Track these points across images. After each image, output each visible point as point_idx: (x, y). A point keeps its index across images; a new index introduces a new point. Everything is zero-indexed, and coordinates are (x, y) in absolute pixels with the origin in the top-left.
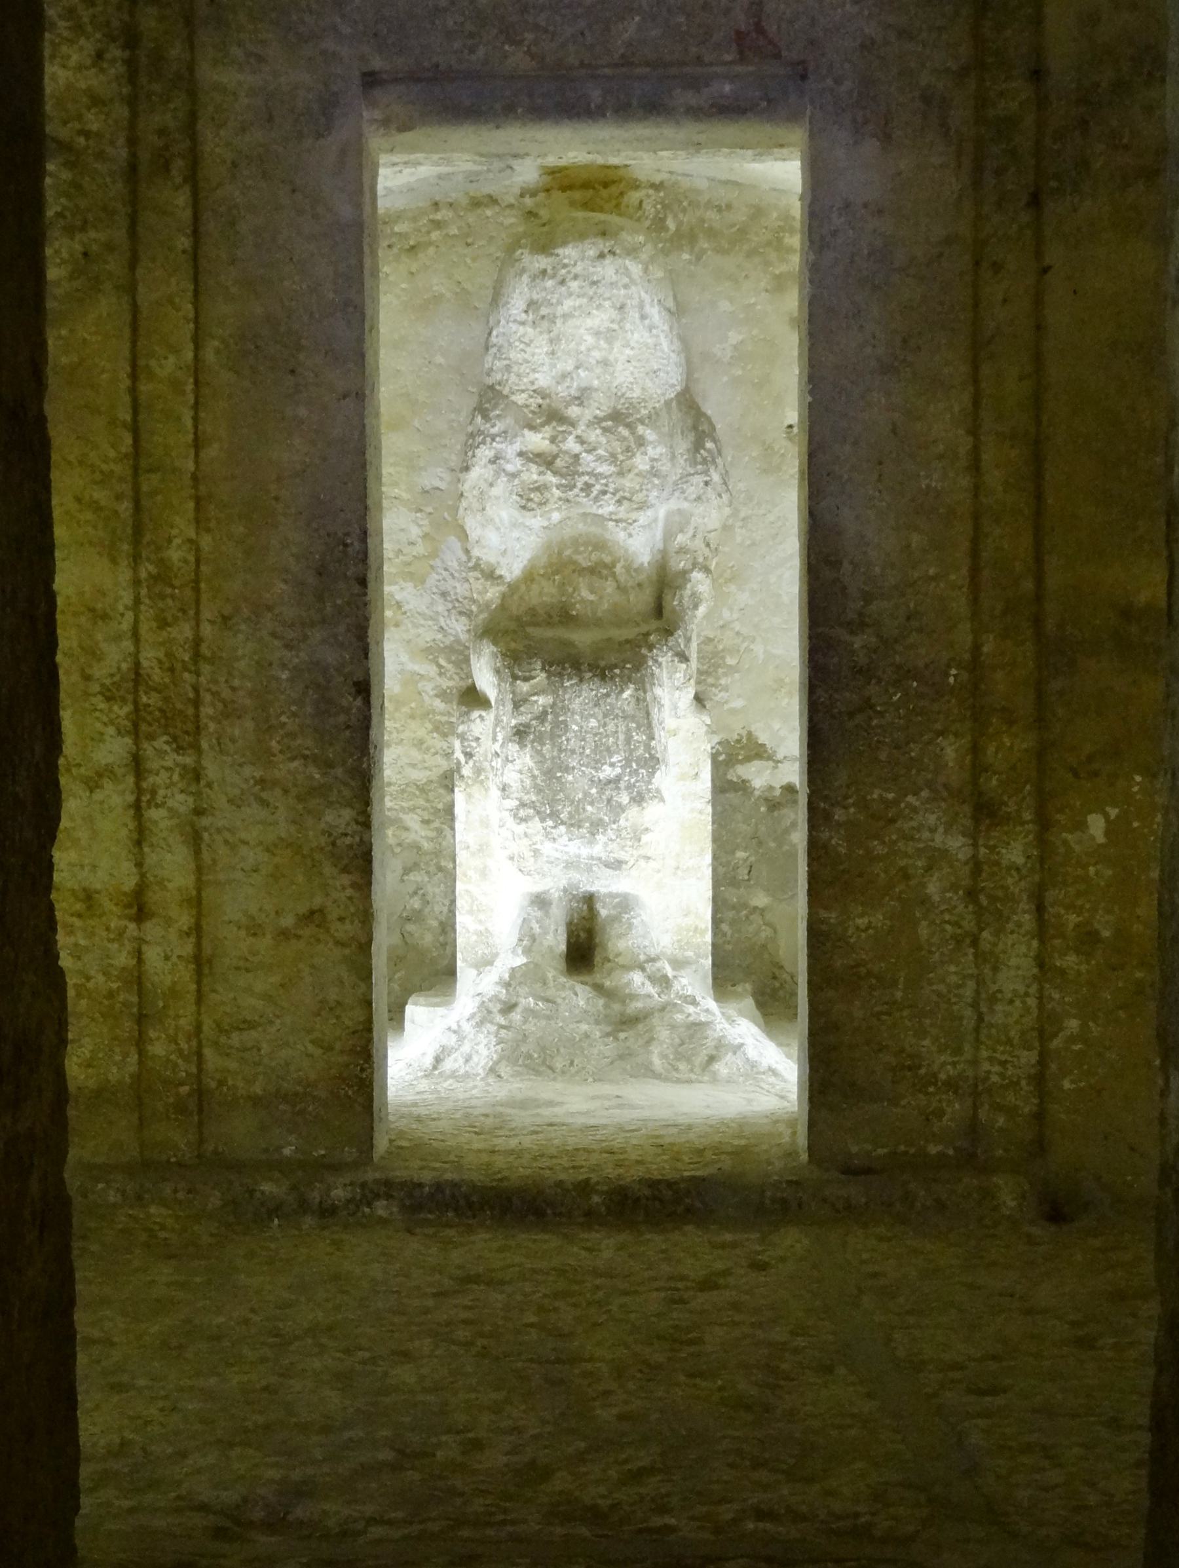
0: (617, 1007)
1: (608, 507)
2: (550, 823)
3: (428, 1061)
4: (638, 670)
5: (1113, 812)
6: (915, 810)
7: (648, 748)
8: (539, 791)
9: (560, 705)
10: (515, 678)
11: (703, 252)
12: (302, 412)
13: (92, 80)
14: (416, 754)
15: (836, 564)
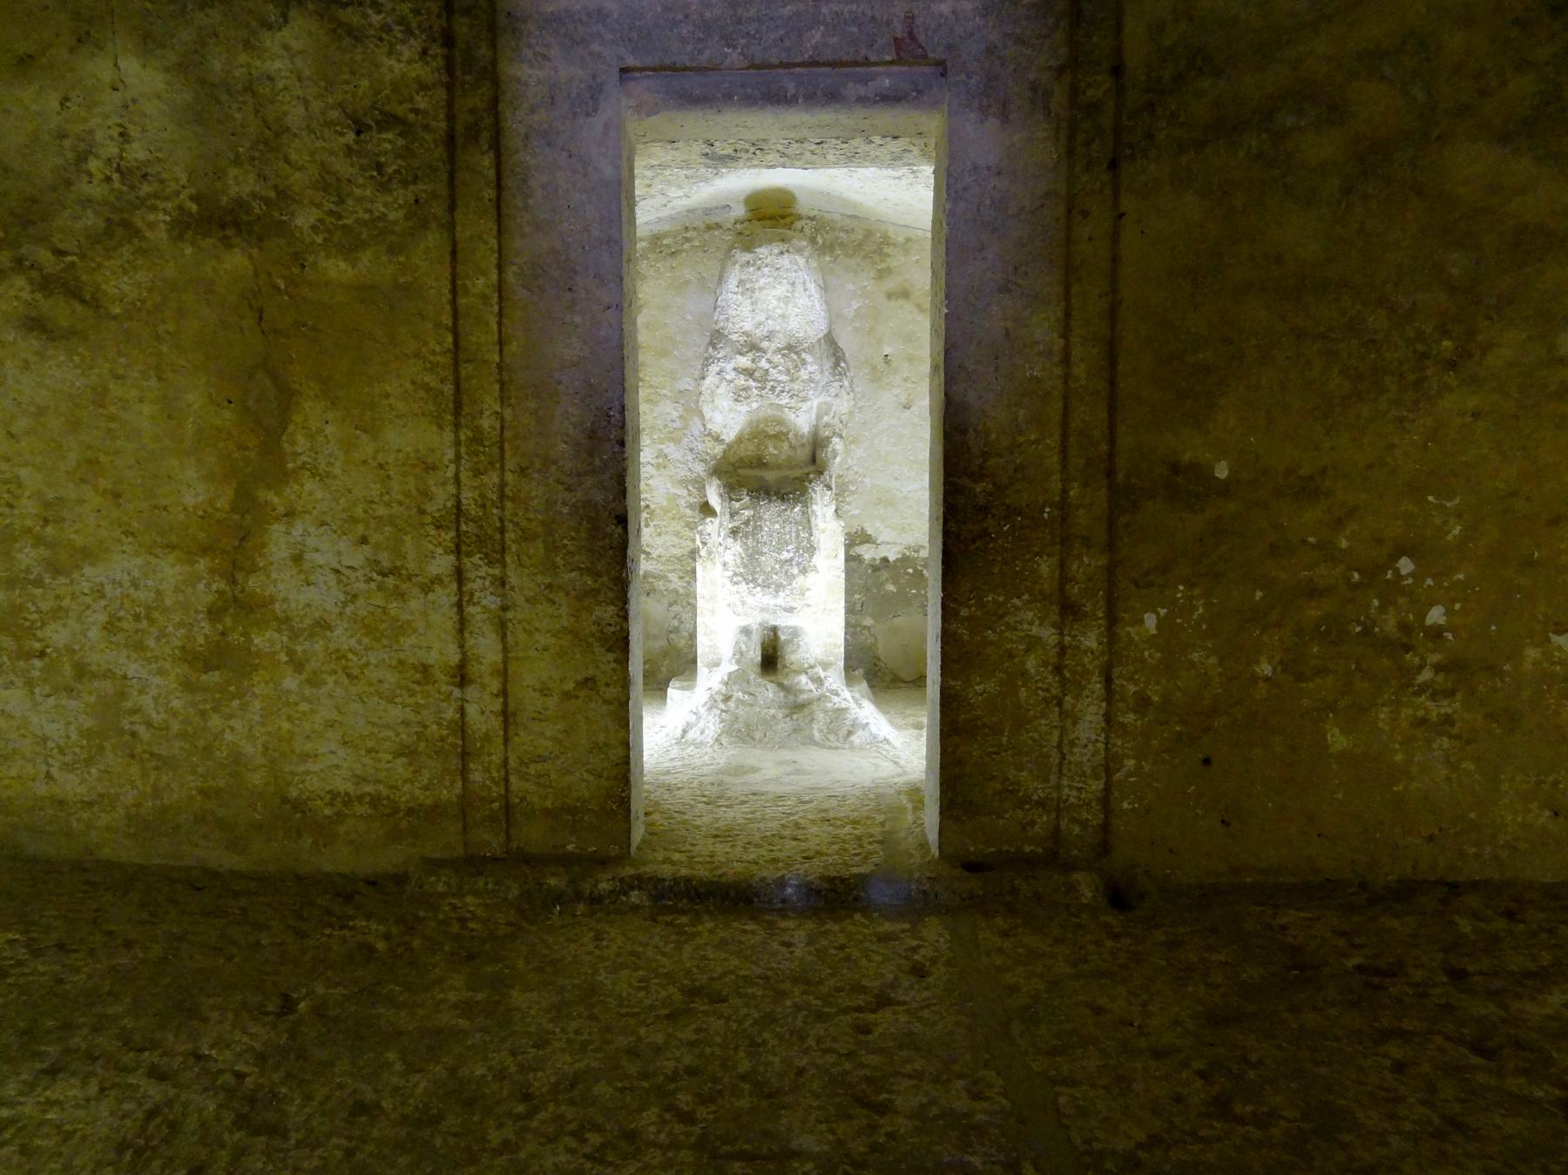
0: (791, 698)
1: (785, 400)
3: (679, 733)
5: (1163, 612)
6: (1018, 609)
7: (809, 541)
8: (745, 566)
12: (578, 319)
13: (419, 71)
14: (676, 540)
15: (964, 432)
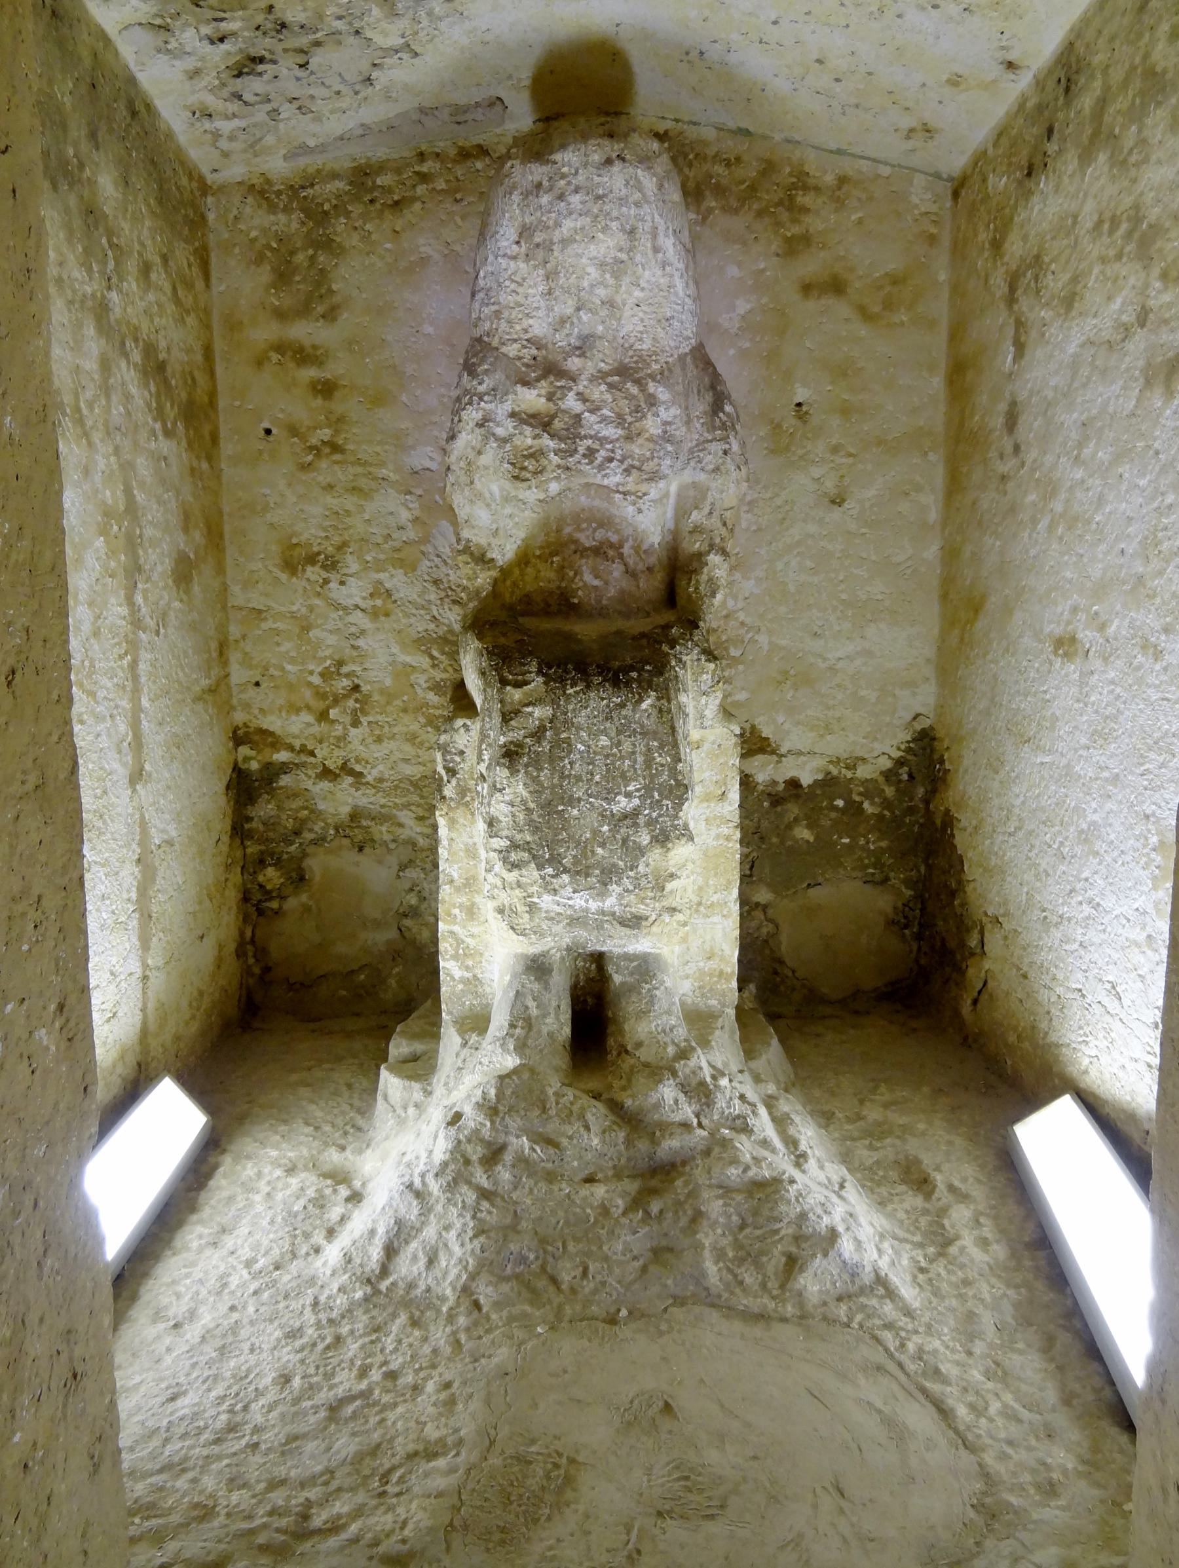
0: (643, 1145)
1: (614, 477)
2: (550, 871)
4: (661, 674)
7: (674, 772)
8: (536, 829)
9: (562, 718)
10: (504, 682)
11: (710, 210)
14: (409, 749)
